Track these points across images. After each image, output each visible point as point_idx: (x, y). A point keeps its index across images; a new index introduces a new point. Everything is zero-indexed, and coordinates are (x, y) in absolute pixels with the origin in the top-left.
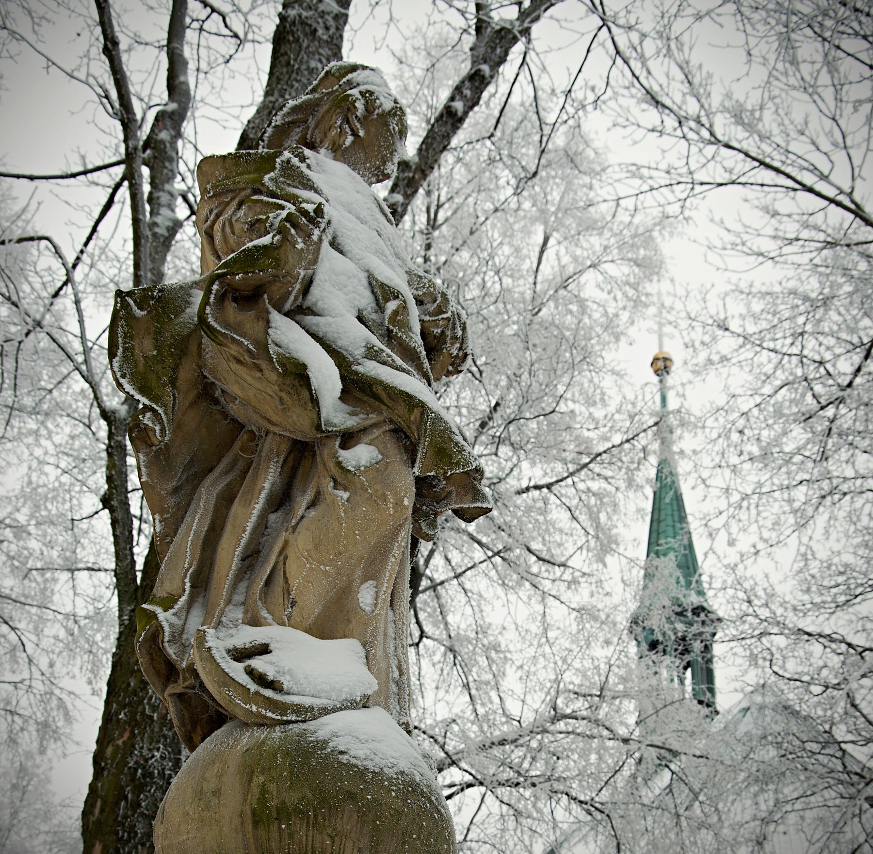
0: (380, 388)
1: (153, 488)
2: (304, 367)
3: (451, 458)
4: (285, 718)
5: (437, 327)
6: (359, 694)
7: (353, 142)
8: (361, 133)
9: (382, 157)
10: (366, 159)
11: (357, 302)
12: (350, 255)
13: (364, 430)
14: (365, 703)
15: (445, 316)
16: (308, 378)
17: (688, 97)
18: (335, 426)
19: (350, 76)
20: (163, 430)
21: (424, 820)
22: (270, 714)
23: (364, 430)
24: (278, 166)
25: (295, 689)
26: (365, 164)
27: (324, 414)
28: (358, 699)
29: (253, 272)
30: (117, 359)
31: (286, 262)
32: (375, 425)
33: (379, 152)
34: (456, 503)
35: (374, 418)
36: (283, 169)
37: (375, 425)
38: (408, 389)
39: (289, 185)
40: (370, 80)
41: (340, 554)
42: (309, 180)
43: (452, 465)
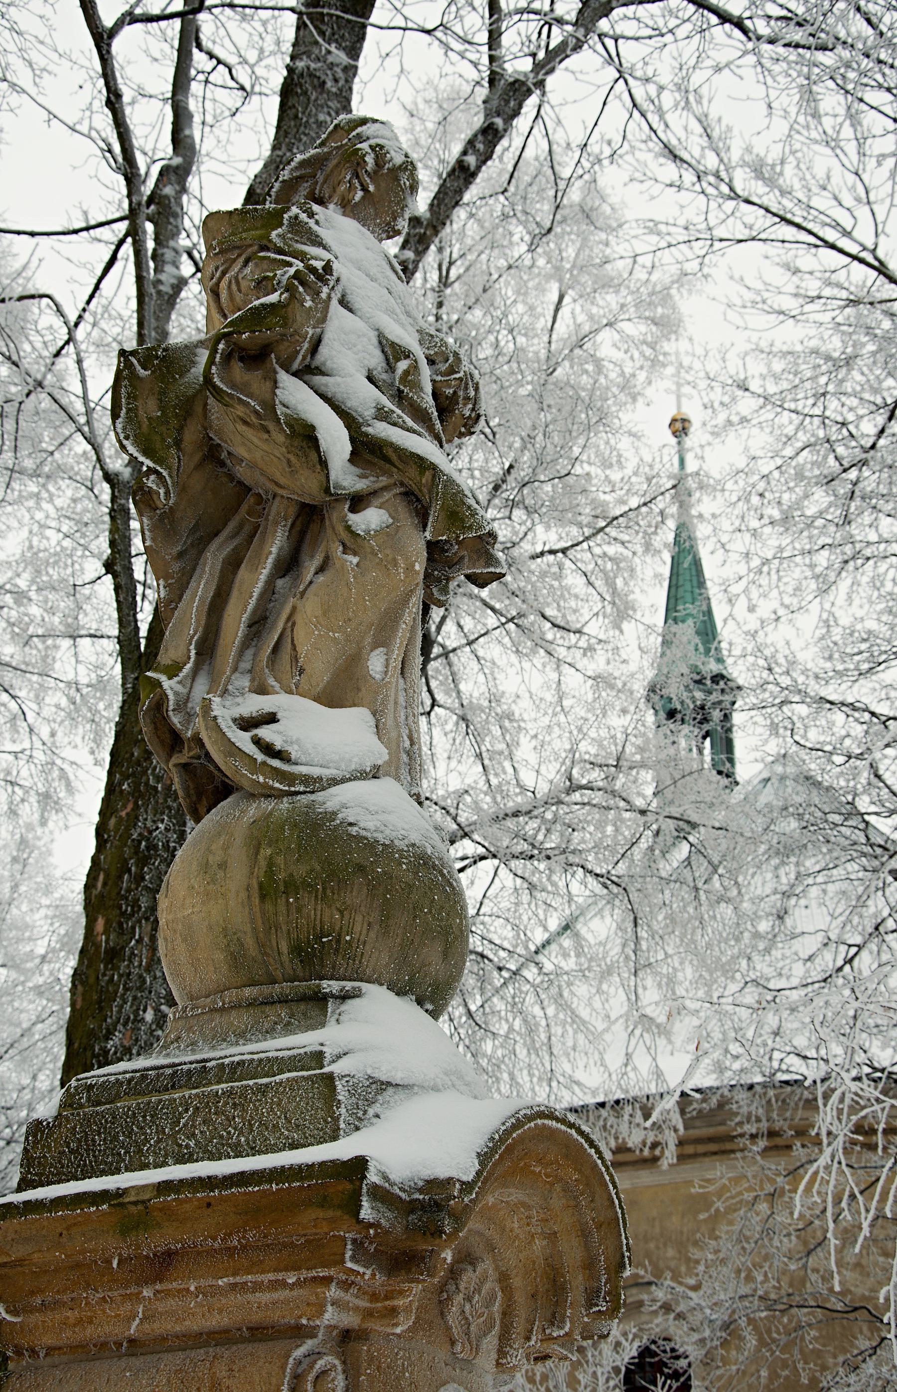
1: (157, 552)
3: (463, 521)
5: (450, 387)
7: (363, 198)
8: (371, 188)
13: (374, 493)
16: (316, 440)
17: (707, 151)
19: (359, 130)
20: (167, 493)
22: (277, 785)
23: (374, 493)
25: (303, 759)
27: (332, 477)
31: (294, 321)
33: (390, 207)
35: (384, 480)
36: (291, 225)
43: (465, 529)
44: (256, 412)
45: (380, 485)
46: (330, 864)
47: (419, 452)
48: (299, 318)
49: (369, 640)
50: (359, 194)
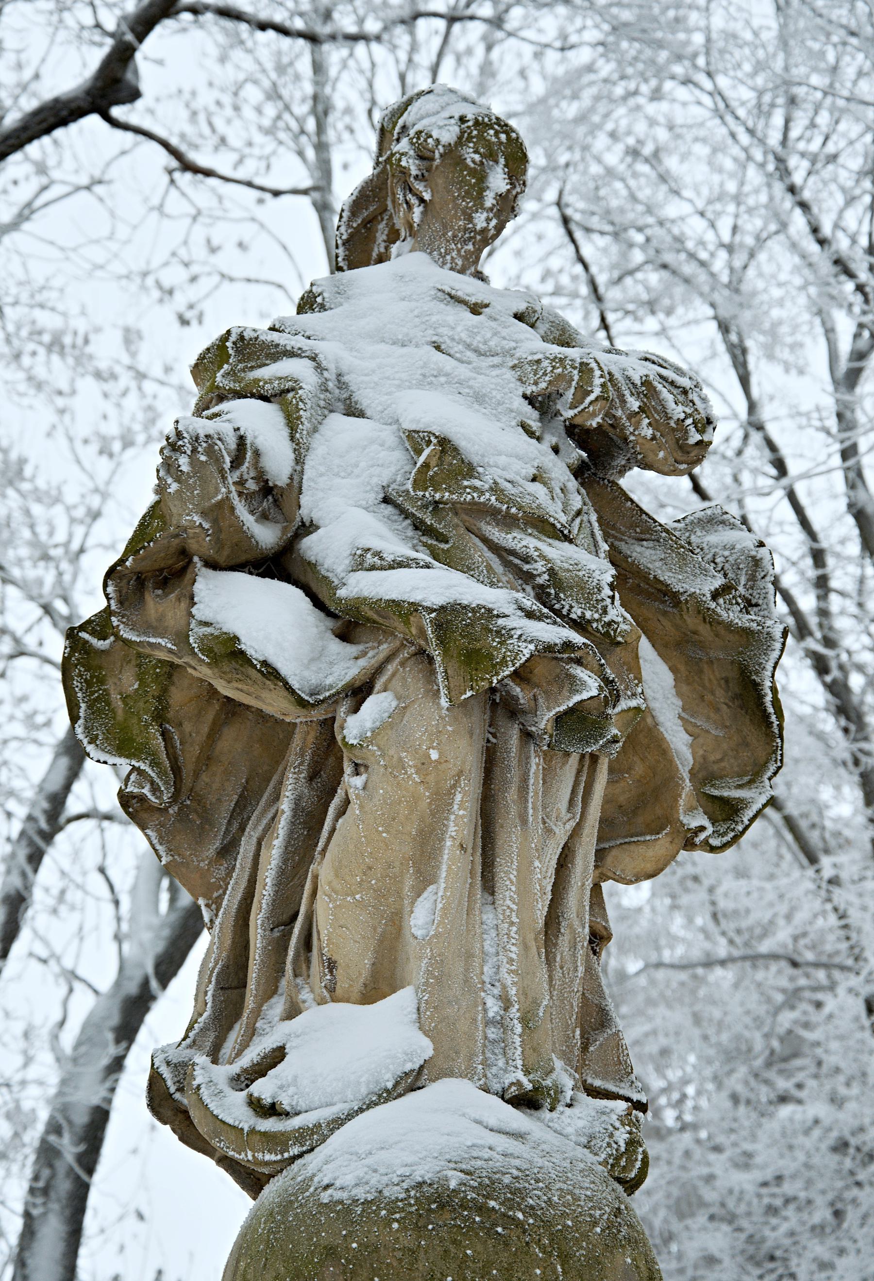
0: (367, 609)
1: (186, 865)
2: (236, 639)
3: (491, 657)
4: (286, 1155)
5: (594, 415)
6: (388, 1076)
7: (424, 214)
8: (427, 196)
9: (464, 213)
10: (445, 226)
11: (375, 480)
12: (368, 413)
13: (379, 670)
14: (411, 1082)
15: (592, 397)
16: (242, 653)
17: (177, 175)
18: (331, 687)
19: (401, 122)
20: (155, 789)
21: (467, 1247)
22: (268, 1157)
23: (379, 670)
24: (231, 351)
25: (302, 1105)
26: (444, 235)
27: (295, 684)
28: (390, 1085)
29: (144, 547)
30: (81, 722)
31: (171, 515)
32: (388, 659)
33: (456, 207)
34: (549, 709)
35: (385, 649)
36: (238, 351)
37: (388, 659)
38: (394, 595)
39: (252, 368)
40: (423, 112)
41: (370, 868)
42: (277, 345)
43: (495, 668)
44: (170, 651)
45: (381, 657)
46: (294, 1259)
47: (394, 596)
48: (174, 510)
49: (409, 882)
50: (417, 211)
